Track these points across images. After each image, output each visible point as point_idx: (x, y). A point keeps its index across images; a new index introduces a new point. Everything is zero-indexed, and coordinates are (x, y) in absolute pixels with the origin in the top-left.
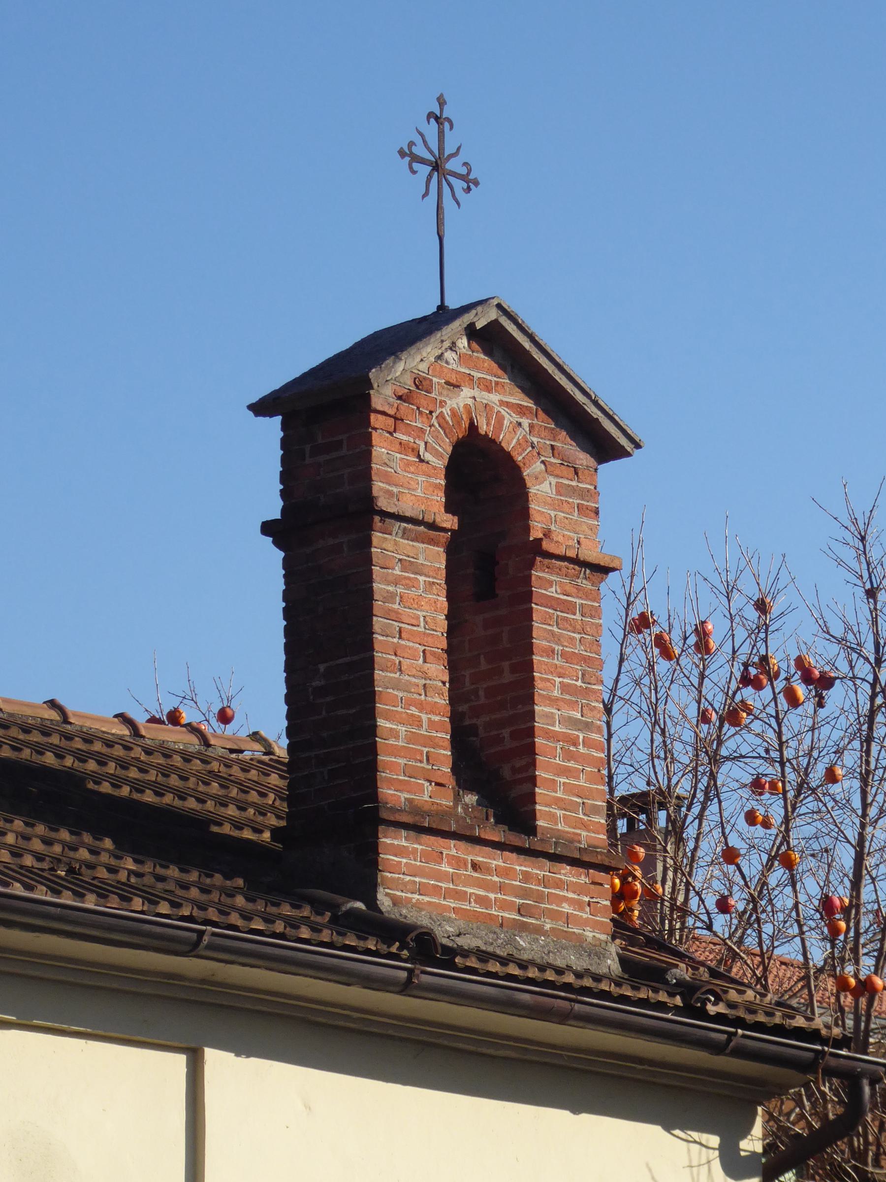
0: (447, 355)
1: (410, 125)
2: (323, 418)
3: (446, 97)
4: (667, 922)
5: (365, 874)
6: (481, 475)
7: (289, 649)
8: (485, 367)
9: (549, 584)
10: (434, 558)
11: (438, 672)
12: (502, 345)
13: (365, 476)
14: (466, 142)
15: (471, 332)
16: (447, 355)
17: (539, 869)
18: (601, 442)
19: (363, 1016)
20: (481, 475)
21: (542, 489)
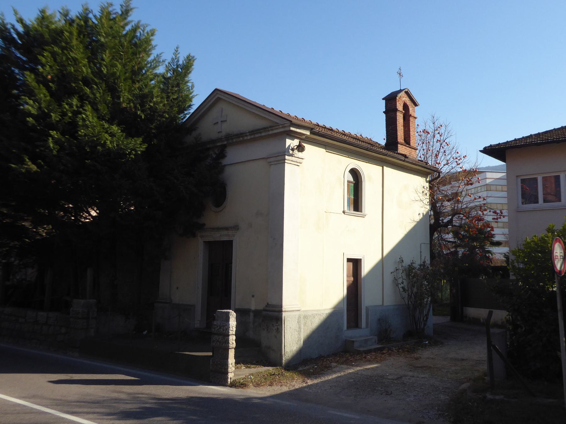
0: (403, 94)
1: (397, 70)
2: (391, 100)
3: (156, 33)
4: (292, 129)
5: (396, 149)
6: (406, 107)
7: (386, 123)
8: (406, 96)
9: (411, 119)
10: (402, 116)
11: (402, 128)
12: (407, 93)
13: (396, 106)
14: (403, 72)
15: (405, 92)
16: (403, 94)
17: (411, 149)
18: (416, 104)
19: (267, 133)
20: (406, 107)
21: (411, 109)
